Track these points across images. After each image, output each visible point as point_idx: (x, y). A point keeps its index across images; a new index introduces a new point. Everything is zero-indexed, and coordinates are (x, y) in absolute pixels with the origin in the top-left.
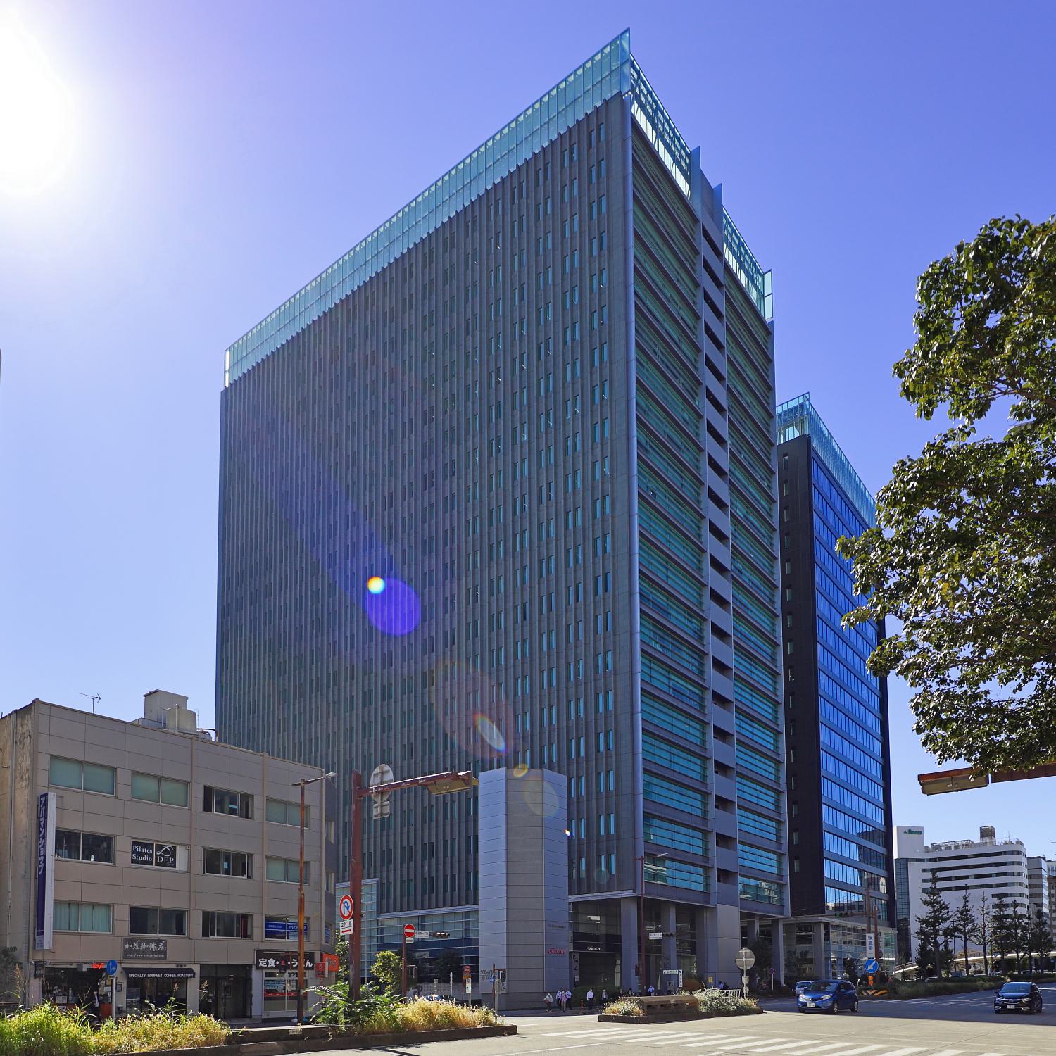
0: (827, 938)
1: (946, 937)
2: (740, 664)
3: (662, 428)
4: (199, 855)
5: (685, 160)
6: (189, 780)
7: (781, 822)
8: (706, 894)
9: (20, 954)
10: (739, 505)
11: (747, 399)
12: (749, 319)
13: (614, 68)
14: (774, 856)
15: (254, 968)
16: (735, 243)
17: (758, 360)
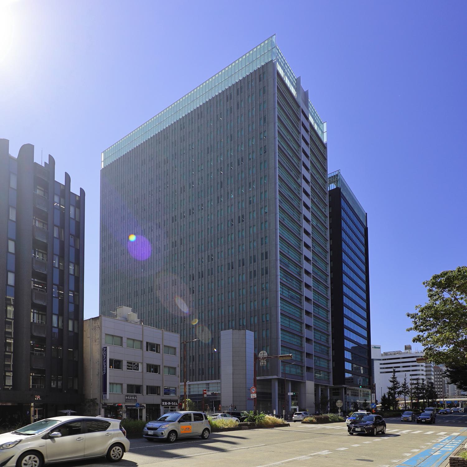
0: (345, 393)
1: (398, 395)
3: (287, 193)
4: (145, 366)
5: (295, 82)
6: (142, 340)
8: (302, 377)
9: (98, 402)
10: (314, 220)
11: (317, 176)
12: (318, 143)
13: (269, 49)
15: (161, 405)
16: (283, 62)
17: (321, 159)
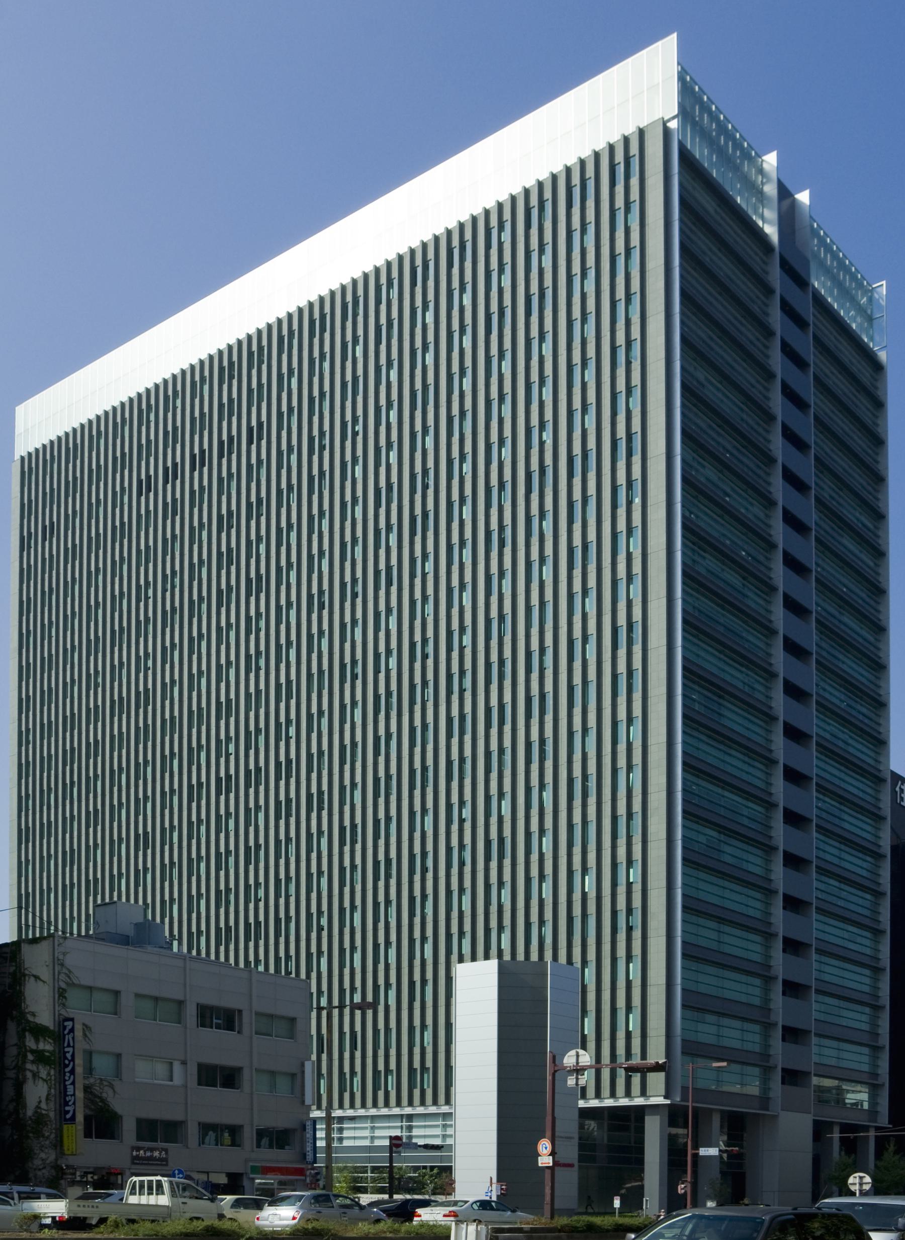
2: (825, 770)
4: (193, 1070)
6: (181, 998)
8: (764, 1100)
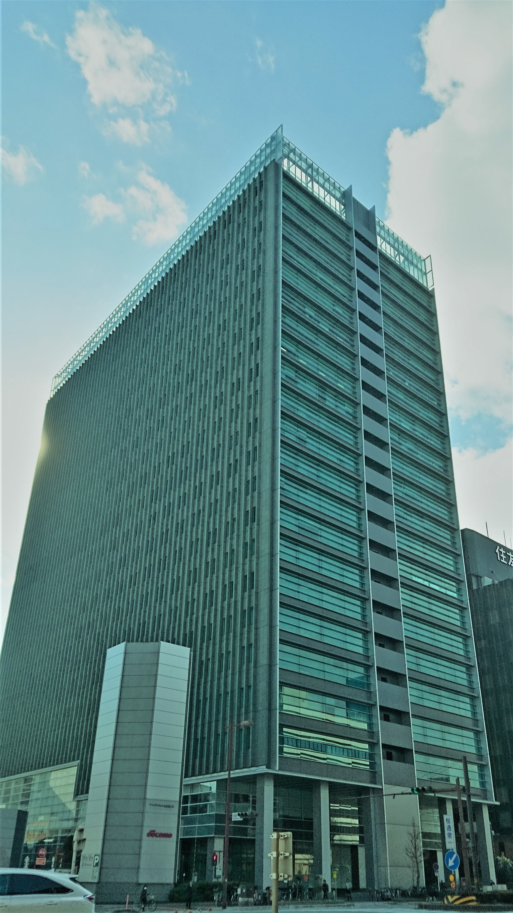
7: (472, 666)
14: (467, 700)
